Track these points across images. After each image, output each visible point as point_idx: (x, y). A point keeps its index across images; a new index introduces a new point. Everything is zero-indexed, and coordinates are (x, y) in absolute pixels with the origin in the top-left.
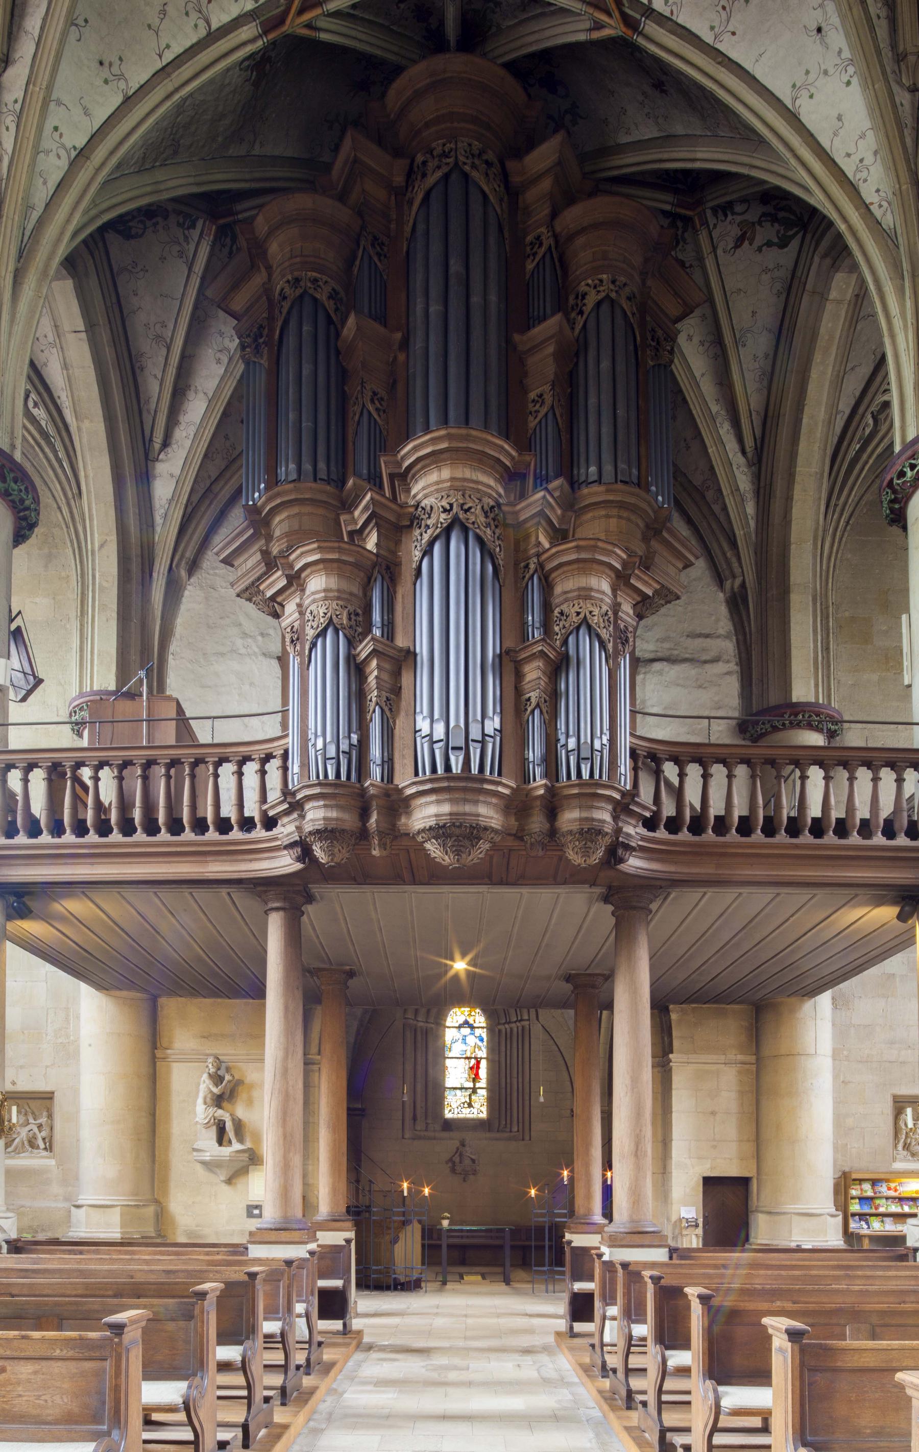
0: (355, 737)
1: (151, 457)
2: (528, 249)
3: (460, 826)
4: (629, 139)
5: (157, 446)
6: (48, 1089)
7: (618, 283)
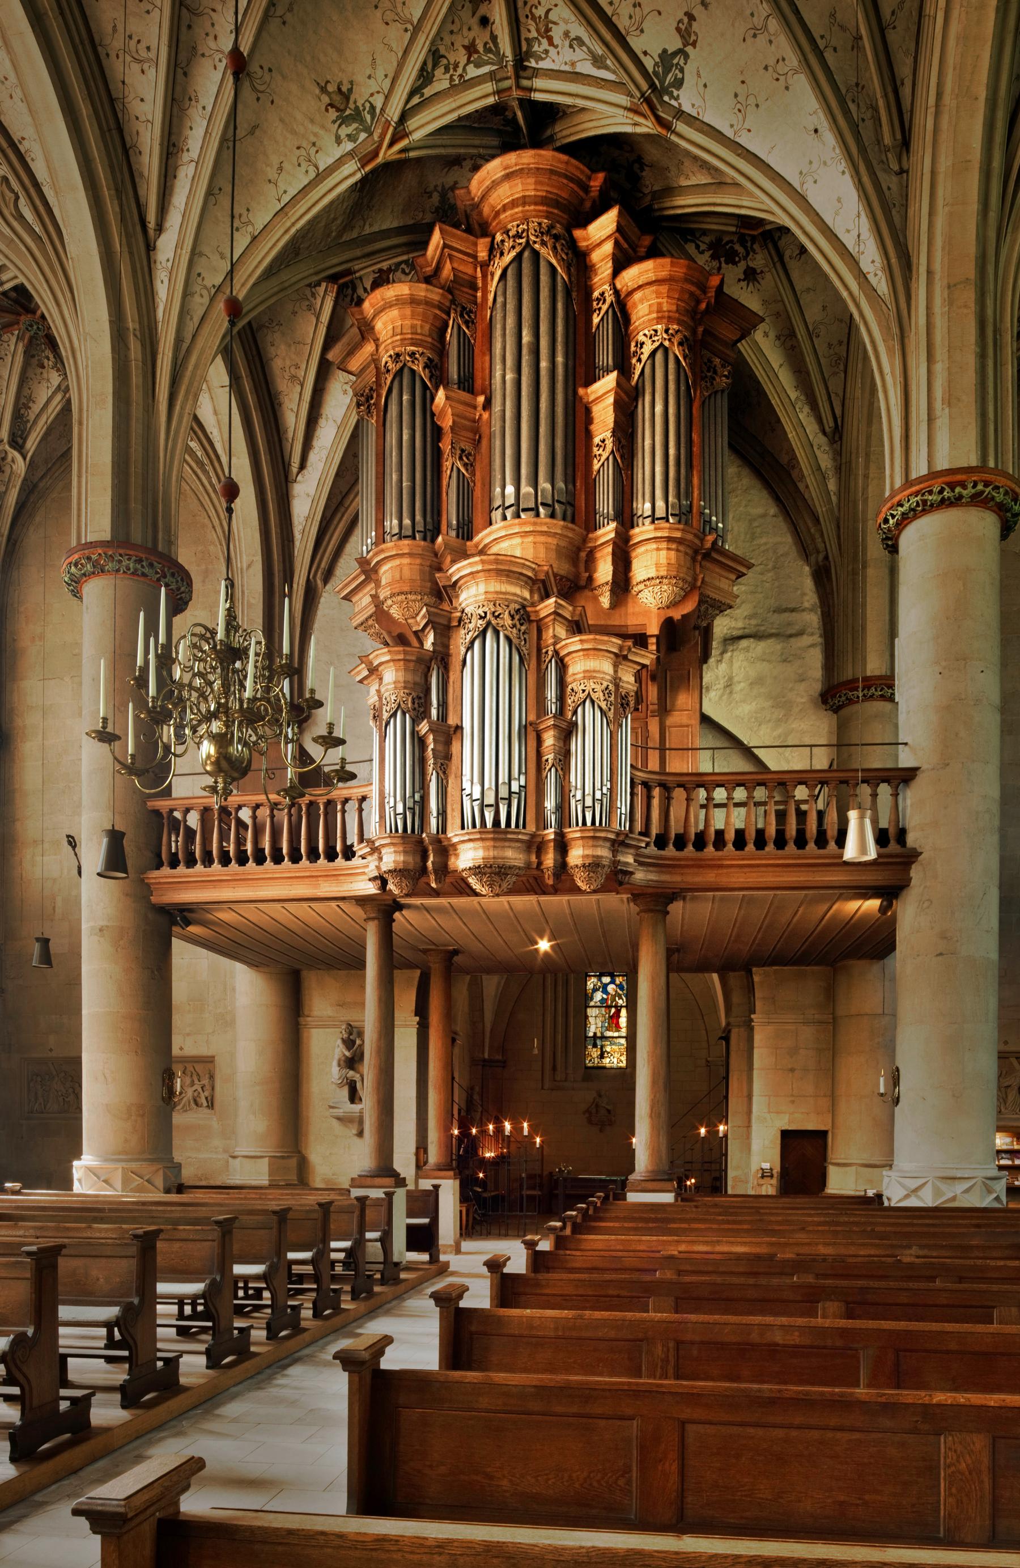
0: (417, 797)
1: (290, 479)
2: (595, 303)
3: (491, 867)
6: (210, 1054)
7: (671, 331)
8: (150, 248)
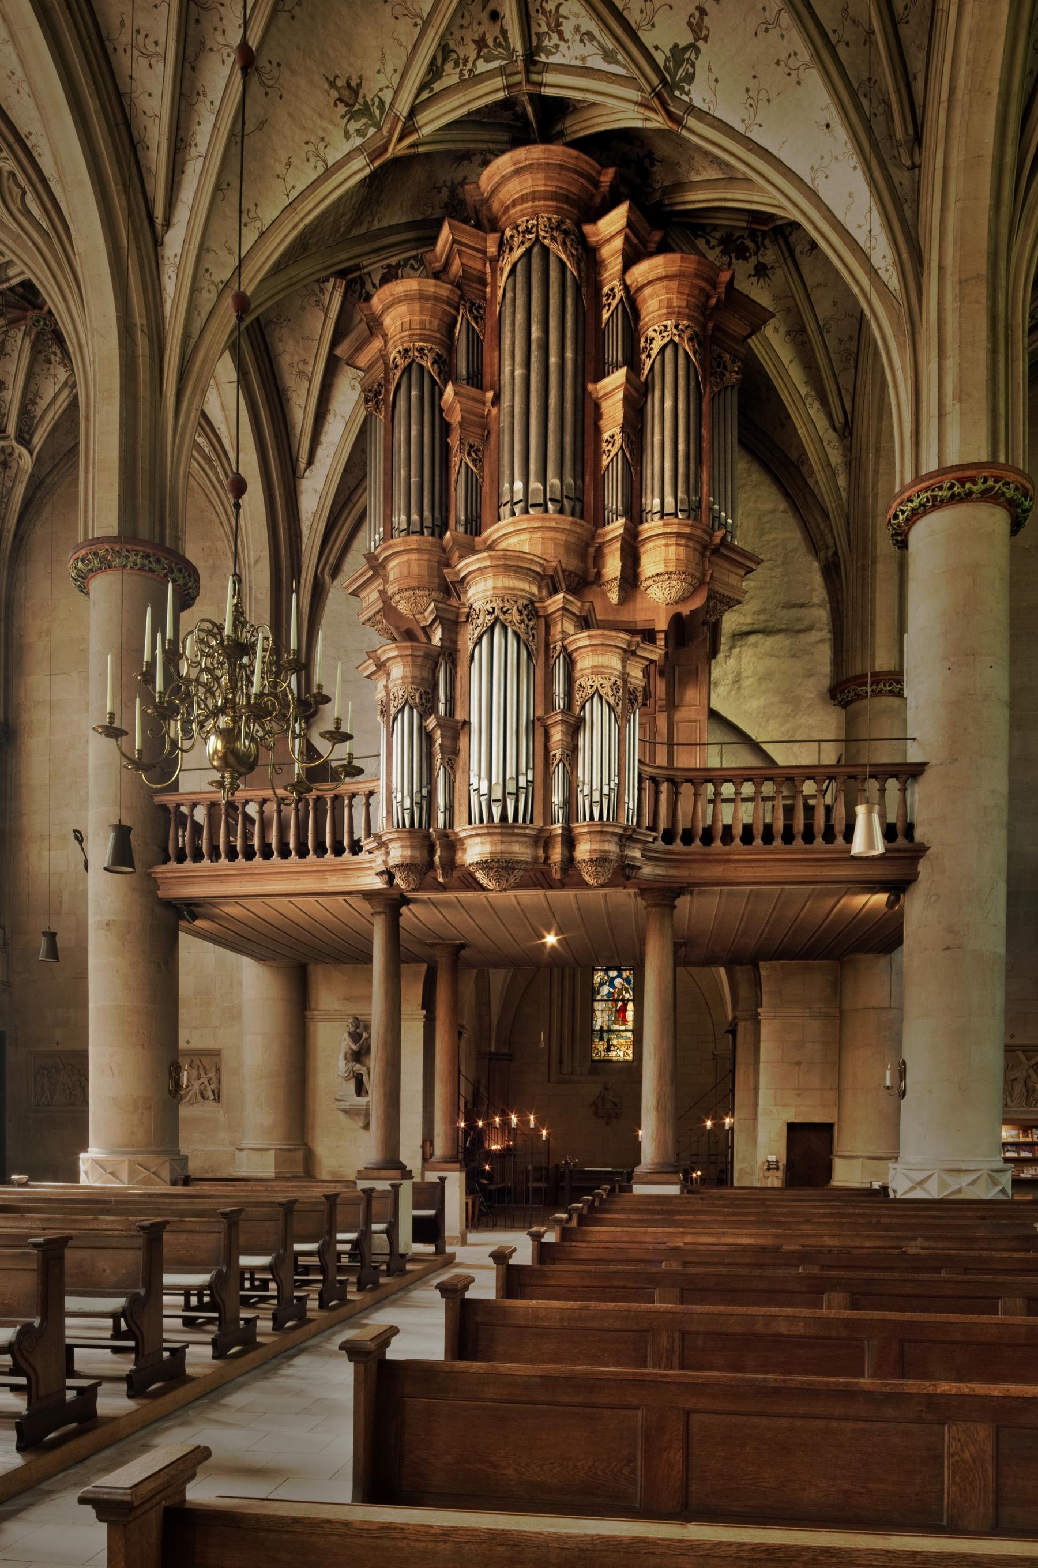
0: (424, 792)
1: (298, 475)
2: (604, 299)
3: (498, 861)
4: (700, 178)
5: (302, 464)
6: (216, 1047)
7: (680, 327)
8: (158, 243)
